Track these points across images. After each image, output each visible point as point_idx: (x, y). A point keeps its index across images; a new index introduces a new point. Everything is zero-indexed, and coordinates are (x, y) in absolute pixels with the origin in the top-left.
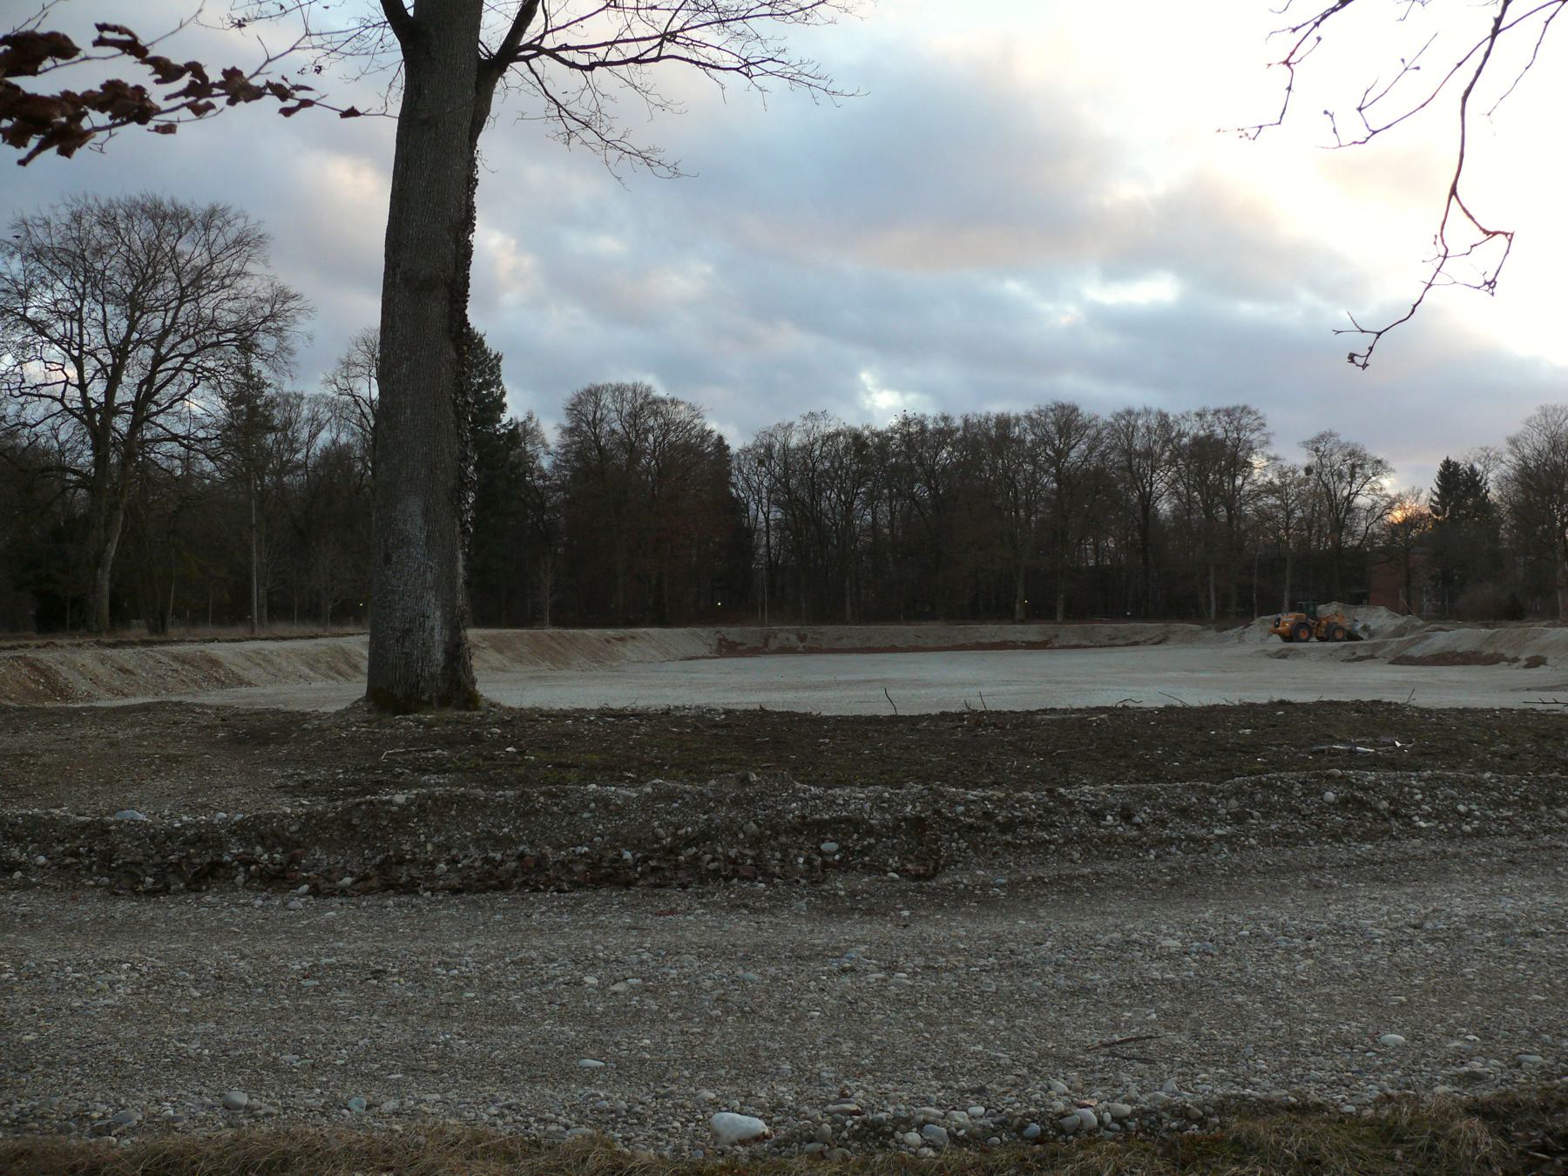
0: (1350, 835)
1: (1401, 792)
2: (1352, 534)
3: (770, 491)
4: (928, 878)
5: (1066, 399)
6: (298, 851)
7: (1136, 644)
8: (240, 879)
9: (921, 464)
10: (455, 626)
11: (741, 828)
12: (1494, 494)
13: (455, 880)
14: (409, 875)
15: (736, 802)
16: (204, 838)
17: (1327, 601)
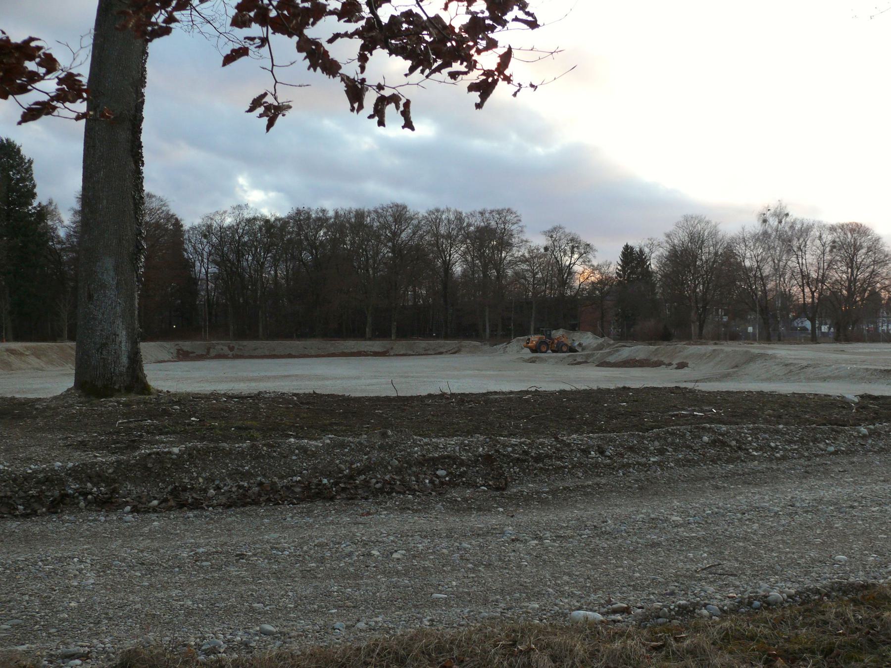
0: (721, 460)
1: (741, 437)
2: (571, 287)
3: (210, 254)
4: (504, 489)
5: (399, 201)
6: (117, 485)
7: (441, 353)
8: (82, 504)
9: (307, 239)
10: (134, 341)
11: (389, 463)
12: (654, 265)
13: (223, 499)
14: (193, 498)
15: (382, 448)
16: (51, 479)
17: (557, 328)
